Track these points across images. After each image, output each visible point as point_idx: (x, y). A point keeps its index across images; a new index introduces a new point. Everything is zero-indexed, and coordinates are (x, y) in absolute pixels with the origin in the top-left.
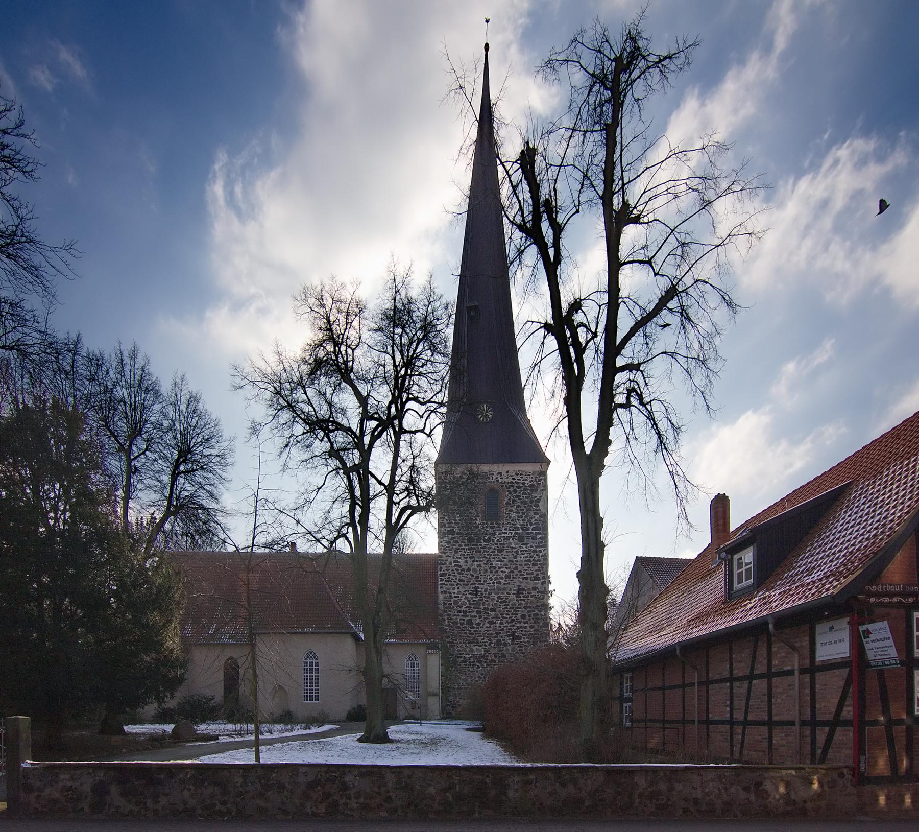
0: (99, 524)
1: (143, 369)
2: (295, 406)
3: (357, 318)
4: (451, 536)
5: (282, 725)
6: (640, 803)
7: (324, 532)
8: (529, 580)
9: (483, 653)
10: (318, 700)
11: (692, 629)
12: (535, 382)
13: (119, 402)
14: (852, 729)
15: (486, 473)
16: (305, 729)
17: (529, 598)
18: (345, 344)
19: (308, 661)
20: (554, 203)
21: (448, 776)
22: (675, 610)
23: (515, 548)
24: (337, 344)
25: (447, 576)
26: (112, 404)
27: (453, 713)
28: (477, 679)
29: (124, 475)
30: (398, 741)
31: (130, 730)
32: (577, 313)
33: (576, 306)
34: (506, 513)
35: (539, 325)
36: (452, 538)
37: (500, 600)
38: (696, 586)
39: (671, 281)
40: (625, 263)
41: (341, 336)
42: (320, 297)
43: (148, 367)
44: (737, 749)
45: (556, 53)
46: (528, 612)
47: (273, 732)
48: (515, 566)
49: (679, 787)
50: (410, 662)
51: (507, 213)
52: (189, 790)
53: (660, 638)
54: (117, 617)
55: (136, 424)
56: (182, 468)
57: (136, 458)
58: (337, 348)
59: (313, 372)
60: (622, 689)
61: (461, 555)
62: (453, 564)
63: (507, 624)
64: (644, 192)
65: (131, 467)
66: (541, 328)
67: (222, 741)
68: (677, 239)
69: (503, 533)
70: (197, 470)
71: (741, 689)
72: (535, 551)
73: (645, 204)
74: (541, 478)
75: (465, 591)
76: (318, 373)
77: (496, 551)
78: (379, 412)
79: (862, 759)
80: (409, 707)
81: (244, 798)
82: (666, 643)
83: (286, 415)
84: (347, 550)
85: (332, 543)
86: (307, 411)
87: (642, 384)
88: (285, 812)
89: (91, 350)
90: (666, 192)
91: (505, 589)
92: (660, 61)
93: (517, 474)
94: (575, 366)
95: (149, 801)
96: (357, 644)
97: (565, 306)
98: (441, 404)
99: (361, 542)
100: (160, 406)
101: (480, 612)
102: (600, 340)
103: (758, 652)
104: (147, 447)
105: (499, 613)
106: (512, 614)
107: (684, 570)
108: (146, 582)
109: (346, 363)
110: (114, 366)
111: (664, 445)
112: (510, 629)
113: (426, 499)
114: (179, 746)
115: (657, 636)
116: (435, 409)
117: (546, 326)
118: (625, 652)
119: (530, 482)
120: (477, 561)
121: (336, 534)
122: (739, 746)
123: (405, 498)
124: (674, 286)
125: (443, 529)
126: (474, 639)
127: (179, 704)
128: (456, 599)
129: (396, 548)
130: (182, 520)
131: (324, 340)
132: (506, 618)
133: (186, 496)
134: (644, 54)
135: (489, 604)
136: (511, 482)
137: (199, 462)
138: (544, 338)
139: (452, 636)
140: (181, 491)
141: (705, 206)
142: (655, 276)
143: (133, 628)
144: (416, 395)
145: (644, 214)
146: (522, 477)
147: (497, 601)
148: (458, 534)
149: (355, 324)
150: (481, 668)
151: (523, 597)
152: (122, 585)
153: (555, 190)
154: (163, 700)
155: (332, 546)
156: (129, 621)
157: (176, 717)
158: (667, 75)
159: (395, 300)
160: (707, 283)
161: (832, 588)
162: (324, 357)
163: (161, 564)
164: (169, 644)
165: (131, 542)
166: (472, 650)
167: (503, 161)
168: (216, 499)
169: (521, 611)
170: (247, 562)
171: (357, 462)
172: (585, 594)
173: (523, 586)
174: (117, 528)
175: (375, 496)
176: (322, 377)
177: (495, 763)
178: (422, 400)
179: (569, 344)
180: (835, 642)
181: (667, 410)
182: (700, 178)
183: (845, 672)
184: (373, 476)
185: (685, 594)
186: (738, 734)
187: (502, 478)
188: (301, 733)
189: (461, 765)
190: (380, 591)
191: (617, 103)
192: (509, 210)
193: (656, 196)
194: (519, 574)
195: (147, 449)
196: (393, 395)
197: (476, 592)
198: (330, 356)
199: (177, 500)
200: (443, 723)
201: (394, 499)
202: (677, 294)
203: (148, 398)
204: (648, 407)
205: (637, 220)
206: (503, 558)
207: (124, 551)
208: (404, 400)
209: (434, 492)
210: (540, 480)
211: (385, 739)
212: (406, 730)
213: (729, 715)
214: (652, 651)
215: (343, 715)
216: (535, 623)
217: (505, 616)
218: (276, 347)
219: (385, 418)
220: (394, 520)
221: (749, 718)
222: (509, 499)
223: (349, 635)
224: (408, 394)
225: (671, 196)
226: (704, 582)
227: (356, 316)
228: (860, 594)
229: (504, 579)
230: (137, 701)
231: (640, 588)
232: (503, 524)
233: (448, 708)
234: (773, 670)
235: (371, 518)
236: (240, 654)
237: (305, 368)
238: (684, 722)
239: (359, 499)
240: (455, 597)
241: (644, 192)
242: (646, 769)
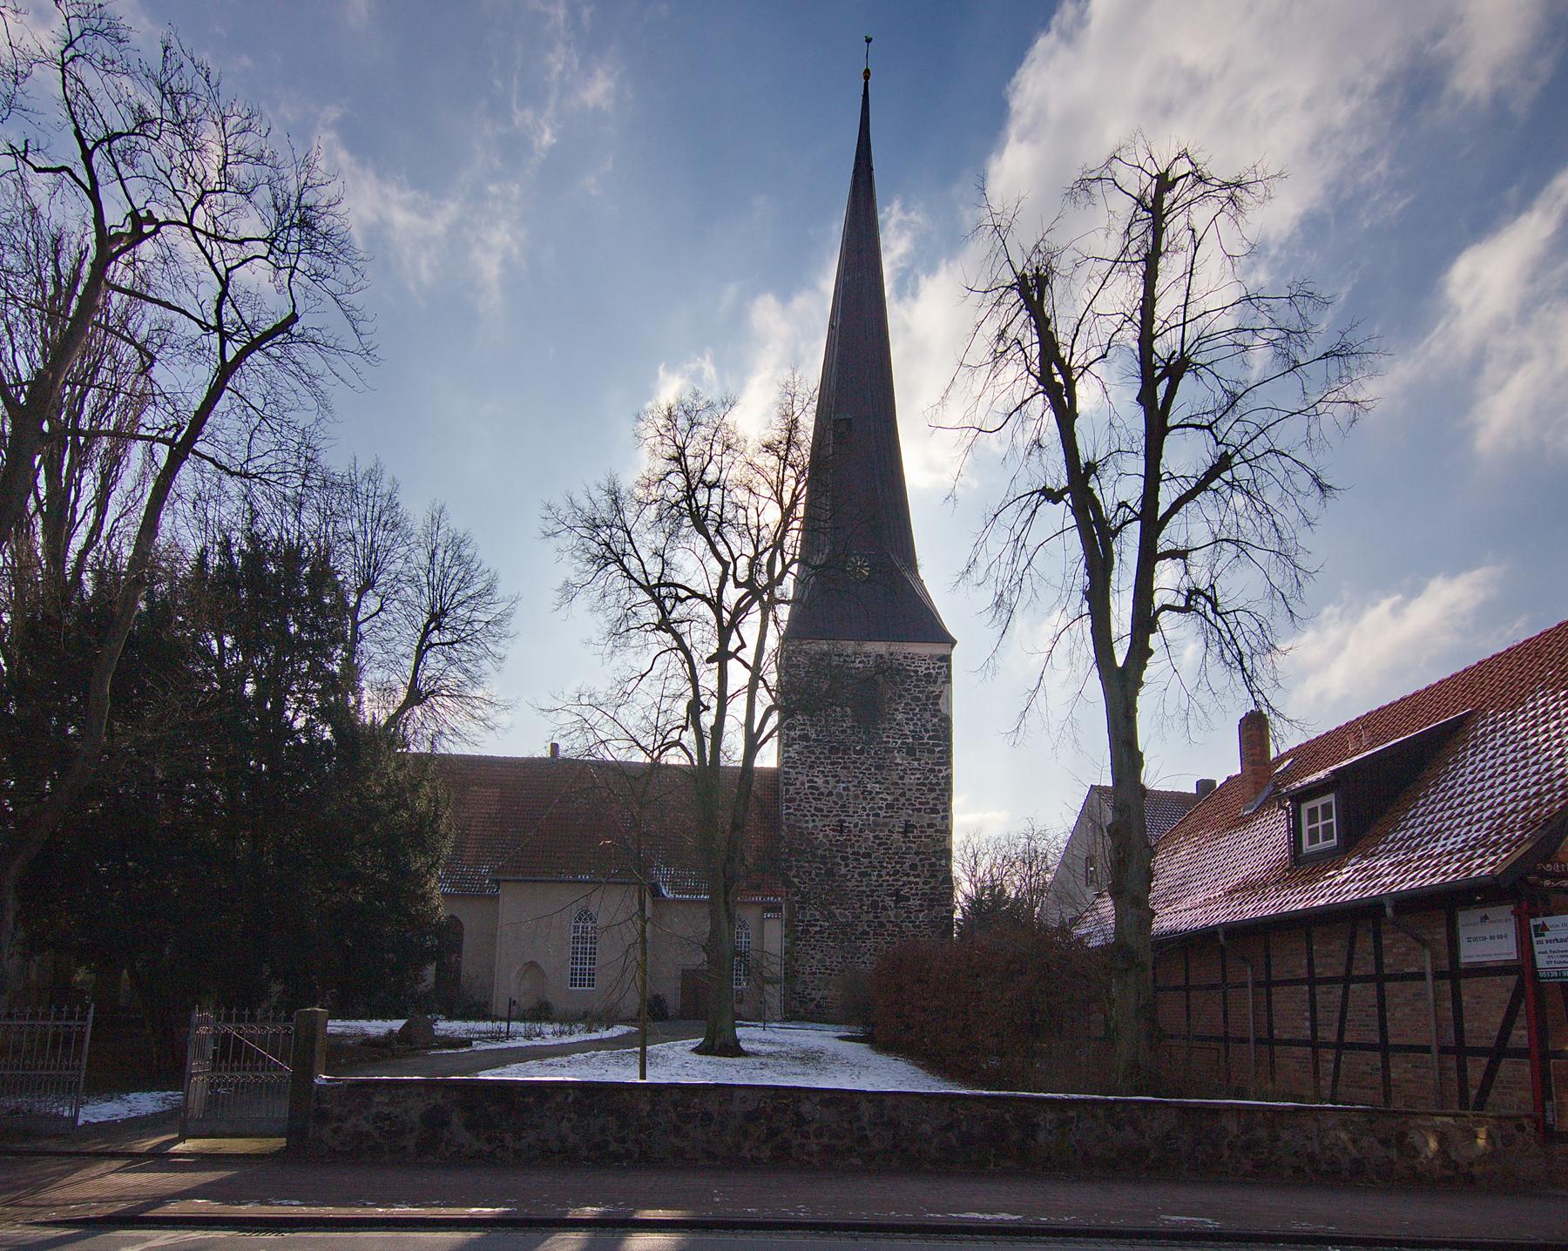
6: (1230, 1157)
8: (923, 813)
10: (593, 985)
14: (1528, 1061)
16: (589, 1031)
19: (581, 925)
25: (797, 802)
44: (1326, 1083)
52: (570, 1120)
71: (1329, 997)
75: (824, 826)
79: (1548, 1105)
91: (885, 825)
95: (508, 1137)
103: (1358, 945)
107: (1191, 814)
112: (893, 885)
119: (926, 669)
120: (843, 782)
122: (1329, 1079)
135: (860, 847)
151: (914, 837)
161: (1483, 867)
173: (913, 820)
180: (1492, 938)
183: (1512, 980)
186: (1327, 1061)
188: (583, 1039)
194: (907, 803)
197: (840, 828)
211: (732, 1049)
213: (1309, 1032)
216: (931, 876)
217: (885, 865)
221: (1347, 1038)
228: (1529, 874)
233: (793, 1003)
234: (1386, 972)
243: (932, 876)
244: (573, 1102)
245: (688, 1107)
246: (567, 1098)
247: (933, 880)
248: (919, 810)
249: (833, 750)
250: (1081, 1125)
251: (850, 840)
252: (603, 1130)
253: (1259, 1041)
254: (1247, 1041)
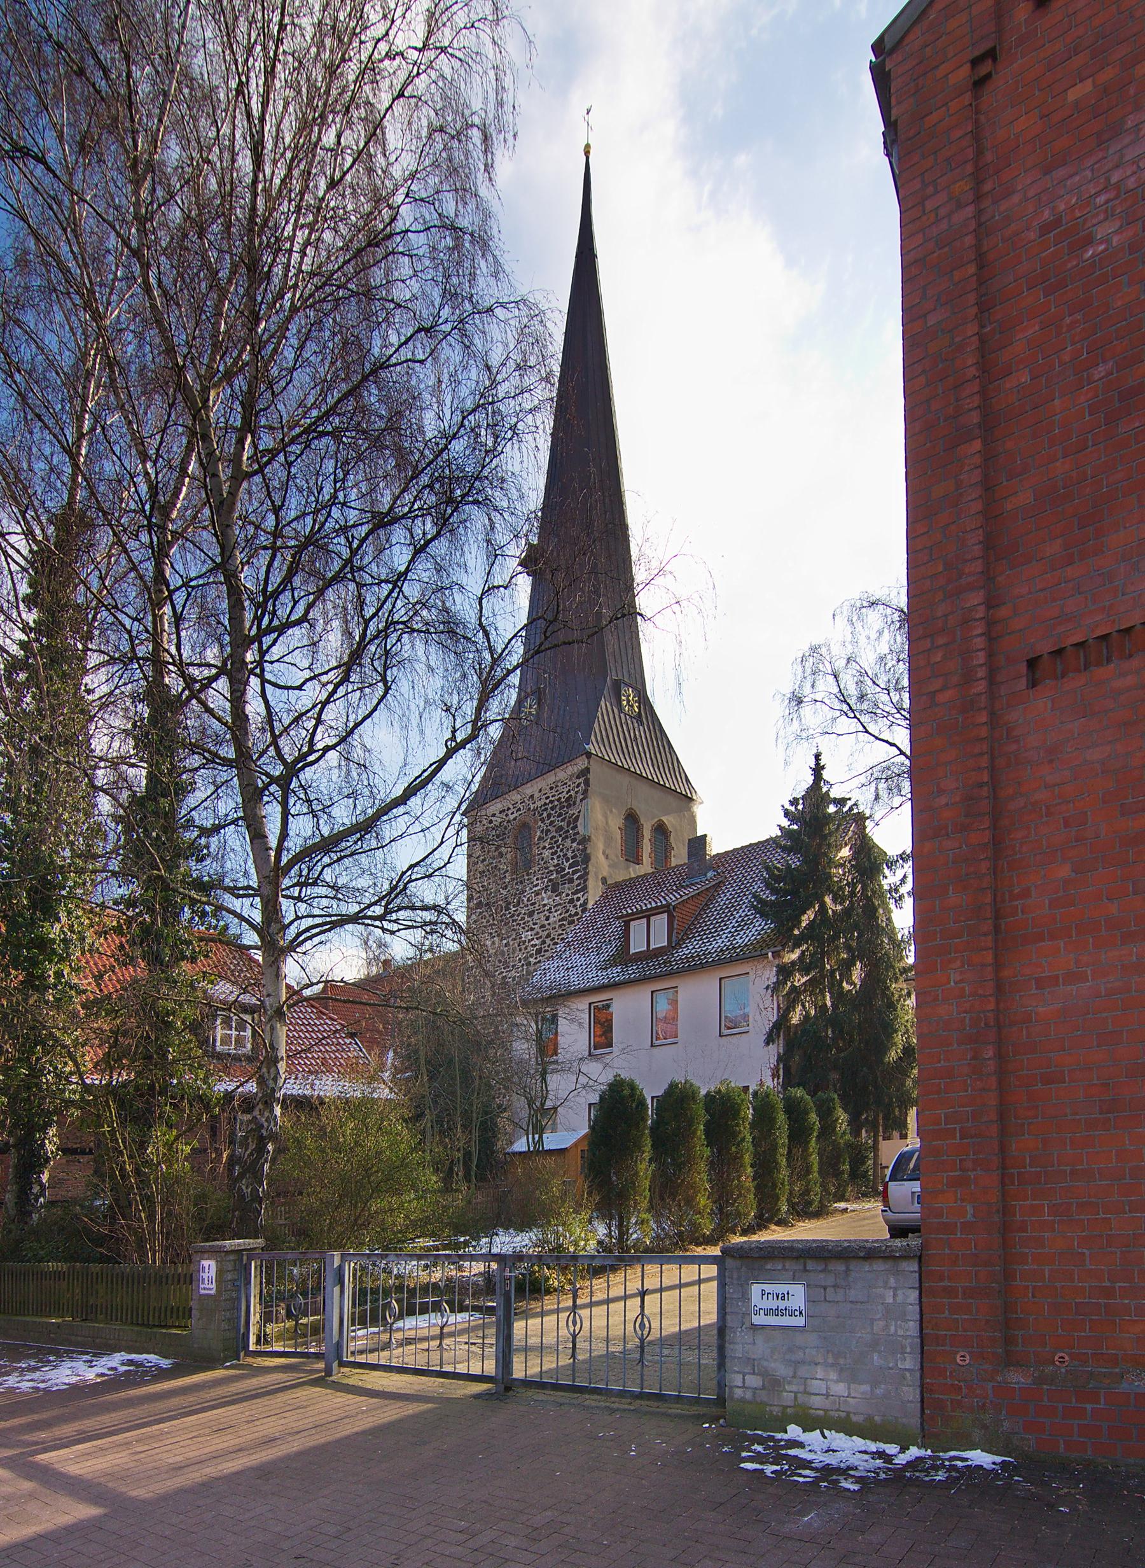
72: (571, 901)
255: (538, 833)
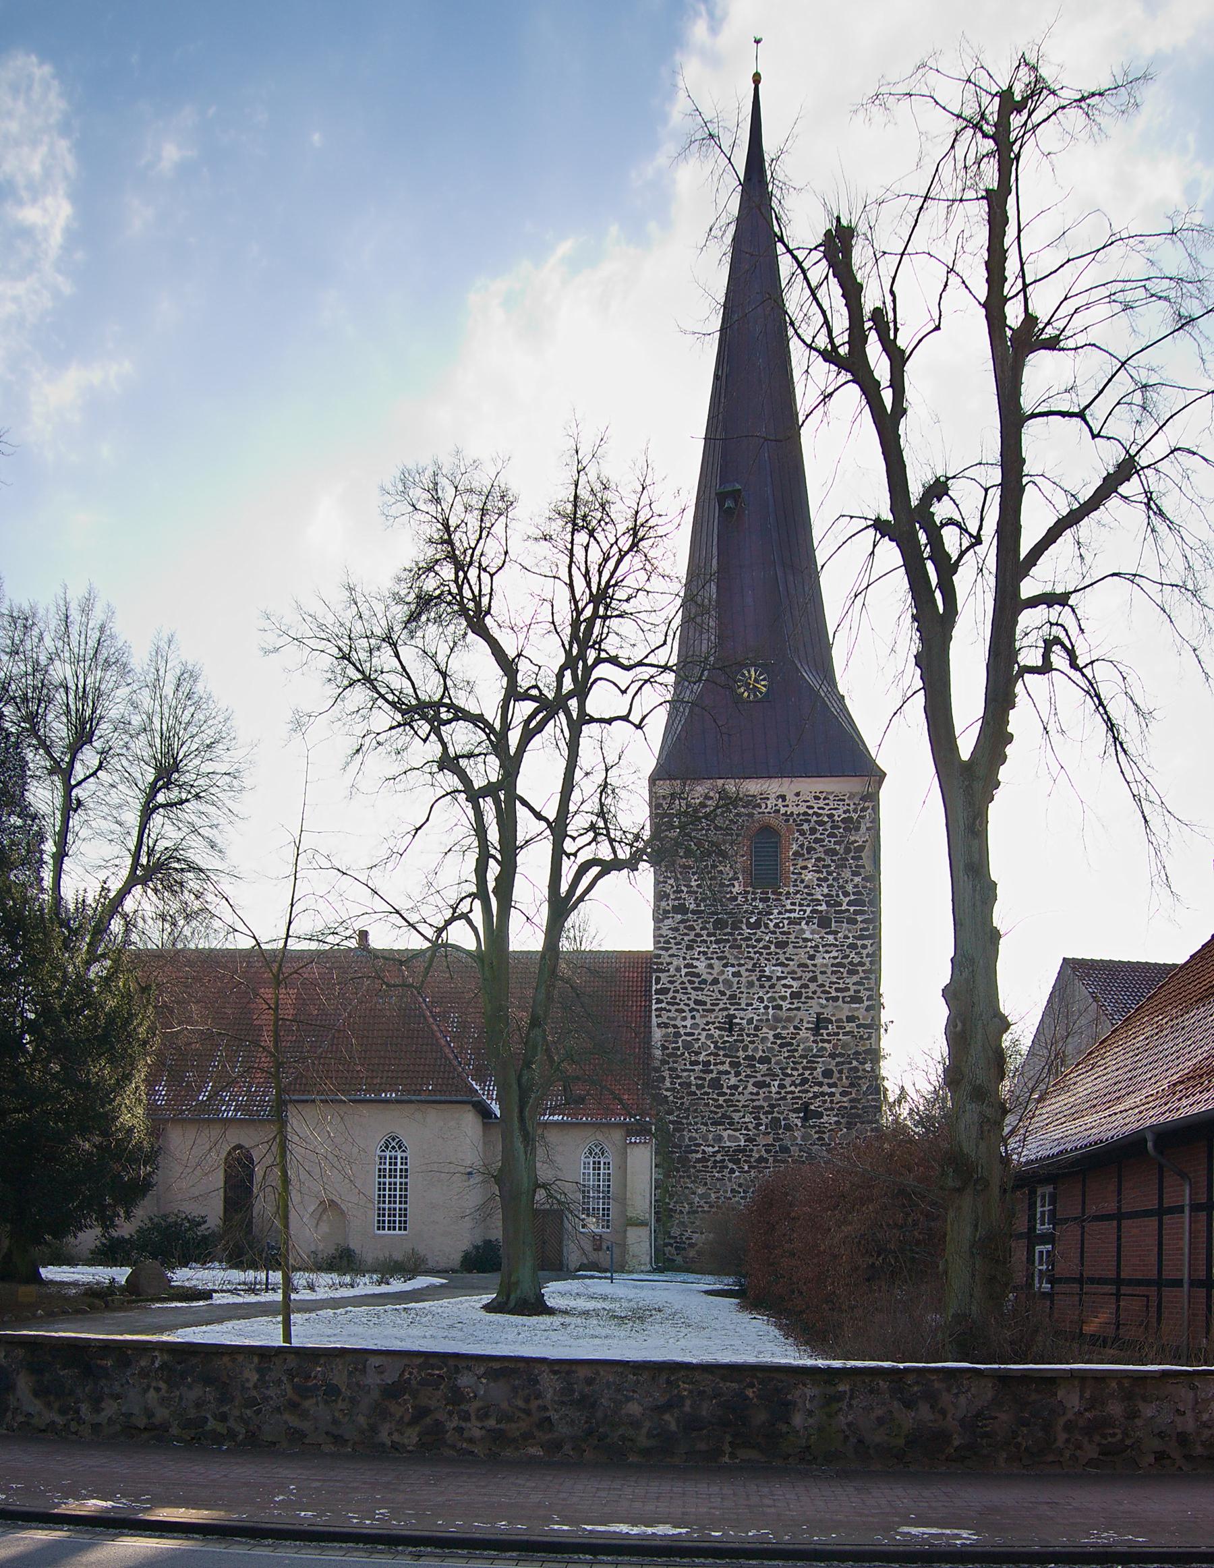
0: (11, 903)
1: (102, 629)
2: (376, 679)
3: (503, 518)
4: (679, 916)
5: (334, 1276)
6: (1067, 1441)
7: (426, 911)
9: (742, 1143)
11: (1179, 1100)
12: (855, 626)
13: (57, 688)
15: (754, 796)
16: (380, 1283)
17: (841, 1037)
18: (477, 565)
19: (388, 1154)
20: (891, 315)
21: (668, 1382)
22: (1144, 1062)
23: (810, 940)
24: (459, 566)
25: (671, 994)
26: (45, 691)
27: (679, 1259)
28: (729, 1194)
29: (58, 815)
30: (566, 1312)
31: (51, 1276)
32: (939, 500)
33: (938, 489)
34: (793, 873)
35: (864, 524)
36: (682, 921)
37: (779, 1042)
38: (1187, 1016)
39: (1125, 448)
40: (1034, 416)
41: (470, 551)
42: (431, 486)
43: (111, 625)
45: (889, 84)
46: (838, 1064)
47: (317, 1289)
48: (811, 974)
49: (1148, 1411)
50: (591, 1160)
51: (800, 331)
52: (158, 1390)
53: (1114, 1118)
54: (35, 1070)
55: (83, 724)
56: (161, 798)
57: (79, 783)
58: (461, 574)
59: (413, 617)
60: (1032, 1218)
61: (699, 953)
62: (684, 971)
63: (793, 1088)
64: (1066, 299)
65: (71, 800)
66: (868, 527)
67: (218, 1302)
68: (1132, 377)
69: (787, 911)
70: (187, 800)
72: (853, 946)
73: (1068, 318)
74: (866, 804)
75: (708, 1023)
76: (424, 618)
77: (773, 947)
78: (541, 685)
80: (588, 1247)
81: (258, 1412)
82: (1125, 1128)
83: (360, 695)
84: (469, 943)
85: (440, 931)
86: (399, 687)
87: (1073, 630)
88: (338, 1440)
89: (16, 602)
90: (1108, 300)
91: (789, 1019)
92: (1083, 99)
93: (816, 798)
94: (938, 595)
96: (484, 1124)
97: (915, 491)
98: (665, 668)
99: (497, 933)
100: (128, 690)
101: (739, 1064)
102: (988, 550)
104: (101, 763)
105: (778, 1067)
106: (804, 1068)
107: (1163, 986)
108: (88, 1005)
109: (476, 599)
110: (52, 627)
111: (1121, 744)
113: (631, 846)
114: (138, 1308)
115: (1107, 1113)
116: (652, 677)
117: (879, 525)
118: (1041, 1145)
119: (845, 812)
120: (733, 966)
121: (448, 914)
123: (589, 844)
124: (1132, 458)
125: (663, 904)
126: (724, 1116)
127: (140, 1231)
128: (689, 1038)
129: (568, 938)
130: (156, 891)
131: (437, 561)
132: (792, 1075)
133: (166, 849)
134: (1052, 87)
135: (756, 1049)
136: (805, 814)
137: (192, 786)
138: (875, 546)
139: (679, 1109)
140: (157, 840)
141: (1183, 325)
142: (1093, 438)
143: (62, 1090)
144: (613, 654)
145: (1067, 333)
146: (828, 804)
147: (775, 1043)
148: (693, 912)
149: (498, 529)
150: (737, 1174)
151: (828, 1034)
152: (46, 1012)
153: (892, 293)
154: (112, 1221)
155: (439, 936)
156: (55, 1076)
157: (134, 1254)
158: (1098, 119)
159: (576, 486)
160: (1194, 454)
162: (435, 589)
163: (116, 972)
164: (126, 1118)
165: (63, 933)
166: (719, 1139)
167: (791, 248)
168: (220, 851)
169: (823, 1062)
170: (275, 966)
171: (494, 779)
172: (959, 1028)
173: (827, 1013)
174: (41, 909)
175: (527, 842)
176: (430, 624)
177: (765, 1360)
178: (626, 662)
179: (925, 555)
181: (1124, 678)
182: (1171, 279)
184: (525, 803)
185: (1165, 1033)
187: (787, 806)
188: (370, 1292)
189: (694, 1361)
190: (535, 1022)
191: (1007, 158)
192: (804, 325)
193: (1088, 306)
195: (100, 767)
196: (568, 653)
197: (730, 1025)
198: (447, 588)
199: (149, 855)
200: (656, 1278)
201: (565, 846)
202: (1137, 472)
203: (107, 678)
204: (1087, 671)
205: (1052, 344)
206: (787, 959)
207: (52, 950)
208: (590, 662)
209: (646, 834)
210: (864, 809)
211: (539, 1307)
212: (582, 1290)
214: (1096, 1143)
215: (456, 1258)
216: (852, 1085)
218: (345, 577)
219: (551, 696)
220: (564, 888)
222: (802, 846)
223: (470, 1107)
224: (600, 650)
225: (1117, 307)
226: (1202, 1009)
227: (500, 514)
229: (789, 1000)
230: (65, 1225)
231: (1071, 1019)
232: (788, 893)
233: (667, 1249)
235: (519, 881)
236: (257, 1141)
237: (400, 612)
238: (1159, 1283)
239: (495, 848)
240: (686, 1034)
241: (1066, 299)
242: (1082, 1376)
243: (852, 1085)
244: (161, 1368)
245: (308, 1377)
246: (153, 1363)
247: (854, 1091)
248: (836, 999)
249: (720, 924)
250: (854, 1402)
251: (743, 1041)
252: (198, 1405)
253: (1193, 1283)
254: (1178, 1283)
255: (795, 847)
